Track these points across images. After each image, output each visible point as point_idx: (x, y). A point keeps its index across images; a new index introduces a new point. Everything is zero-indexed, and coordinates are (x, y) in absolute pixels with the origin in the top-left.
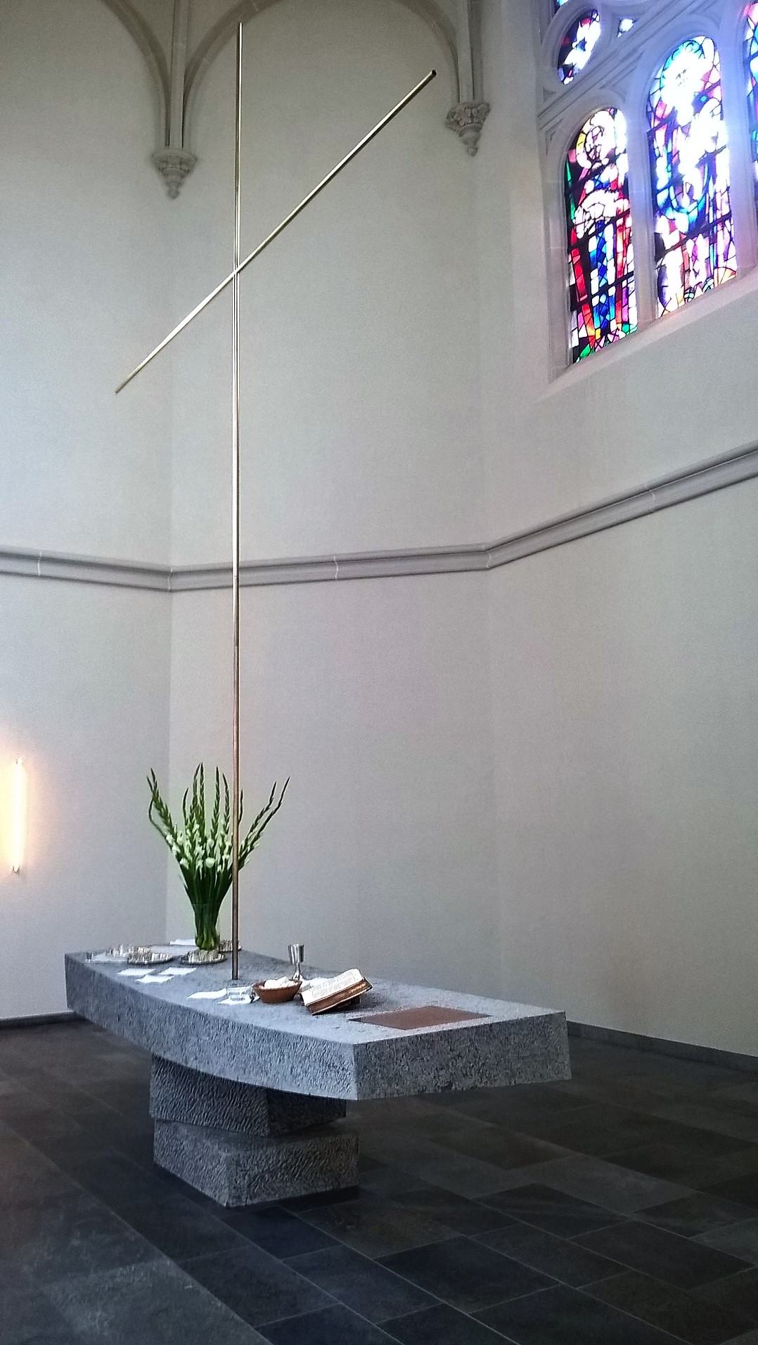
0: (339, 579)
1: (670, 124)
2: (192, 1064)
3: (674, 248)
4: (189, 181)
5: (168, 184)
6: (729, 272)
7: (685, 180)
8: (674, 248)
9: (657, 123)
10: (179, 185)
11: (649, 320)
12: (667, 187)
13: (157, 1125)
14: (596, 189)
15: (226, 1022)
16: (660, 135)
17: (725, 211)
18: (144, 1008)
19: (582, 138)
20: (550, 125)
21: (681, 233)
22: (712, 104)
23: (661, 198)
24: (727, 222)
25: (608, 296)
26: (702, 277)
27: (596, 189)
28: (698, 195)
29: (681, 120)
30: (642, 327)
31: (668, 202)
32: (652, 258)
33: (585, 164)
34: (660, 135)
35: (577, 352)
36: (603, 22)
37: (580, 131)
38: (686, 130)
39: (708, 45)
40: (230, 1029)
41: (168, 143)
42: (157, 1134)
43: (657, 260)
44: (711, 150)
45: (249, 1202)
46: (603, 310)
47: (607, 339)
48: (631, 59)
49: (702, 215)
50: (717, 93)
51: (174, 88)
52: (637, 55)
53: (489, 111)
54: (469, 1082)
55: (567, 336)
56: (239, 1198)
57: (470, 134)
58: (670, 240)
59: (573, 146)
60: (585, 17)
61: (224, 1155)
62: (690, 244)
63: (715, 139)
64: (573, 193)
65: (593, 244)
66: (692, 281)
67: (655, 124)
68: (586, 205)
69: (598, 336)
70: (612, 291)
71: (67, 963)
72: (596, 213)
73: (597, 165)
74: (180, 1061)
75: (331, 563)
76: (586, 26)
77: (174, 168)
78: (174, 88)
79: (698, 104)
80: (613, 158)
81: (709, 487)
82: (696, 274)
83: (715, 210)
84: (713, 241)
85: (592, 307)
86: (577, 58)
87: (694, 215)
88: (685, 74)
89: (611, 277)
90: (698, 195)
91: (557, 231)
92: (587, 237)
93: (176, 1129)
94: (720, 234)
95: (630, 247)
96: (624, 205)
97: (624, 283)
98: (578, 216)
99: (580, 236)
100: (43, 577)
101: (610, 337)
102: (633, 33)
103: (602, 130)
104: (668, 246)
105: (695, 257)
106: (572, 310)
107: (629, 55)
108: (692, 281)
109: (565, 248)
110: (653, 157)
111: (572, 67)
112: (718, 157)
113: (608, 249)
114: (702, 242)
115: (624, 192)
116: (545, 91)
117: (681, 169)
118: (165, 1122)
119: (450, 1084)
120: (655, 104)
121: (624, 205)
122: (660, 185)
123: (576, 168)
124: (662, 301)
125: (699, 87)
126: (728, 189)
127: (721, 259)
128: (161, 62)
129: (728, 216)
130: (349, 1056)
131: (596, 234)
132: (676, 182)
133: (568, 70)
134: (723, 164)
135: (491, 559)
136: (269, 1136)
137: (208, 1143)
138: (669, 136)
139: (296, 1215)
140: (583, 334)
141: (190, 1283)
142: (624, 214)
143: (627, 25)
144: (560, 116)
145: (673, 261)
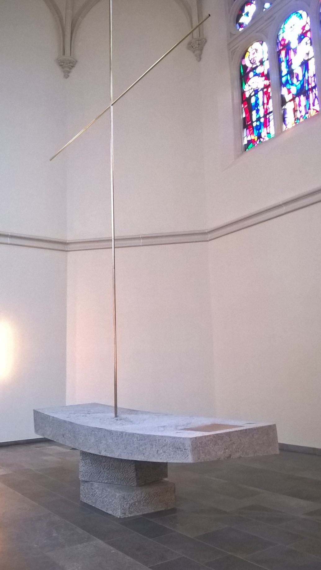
0: (142, 246)
1: (287, 47)
2: (103, 454)
3: (290, 101)
4: (74, 70)
5: (64, 72)
6: (315, 111)
7: (294, 72)
8: (290, 101)
9: (281, 48)
10: (69, 72)
11: (279, 132)
12: (287, 75)
13: (82, 484)
14: (254, 76)
15: (122, 433)
16: (283, 53)
17: (313, 85)
18: (77, 430)
19: (247, 54)
20: (234, 48)
21: (293, 95)
22: (306, 40)
23: (284, 79)
24: (314, 90)
25: (260, 122)
26: (303, 113)
27: (254, 76)
28: (301, 78)
29: (293, 46)
30: (277, 135)
31: (287, 82)
32: (280, 106)
33: (249, 65)
34: (283, 53)
35: (247, 146)
36: (256, 4)
37: (247, 51)
38: (295, 51)
39: (304, 14)
40: (124, 436)
41: (64, 54)
42: (82, 487)
43: (282, 106)
44: (306, 59)
45: (129, 516)
46: (258, 128)
47: (260, 141)
48: (270, 20)
49: (303, 86)
50: (309, 34)
51: (68, 30)
52: (272, 18)
53: (206, 42)
54: (238, 455)
55: (242, 139)
56: (125, 514)
57: (197, 52)
58: (288, 97)
59: (244, 57)
60: (249, 3)
61: (118, 494)
62: (297, 99)
63: (308, 54)
64: (244, 77)
65: (253, 100)
66: (298, 115)
67: (282, 49)
68: (250, 82)
69: (256, 139)
70: (262, 120)
71: (34, 414)
72: (255, 87)
73: (254, 66)
74: (96, 452)
75: (139, 238)
76: (249, 6)
77: (67, 65)
78: (68, 30)
79: (300, 39)
80: (262, 63)
81: (302, 205)
82: (300, 112)
83: (308, 84)
84: (308, 98)
85: (253, 127)
86: (245, 20)
87: (299, 86)
88: (294, 26)
89: (262, 113)
90: (301, 78)
91: (237, 95)
92: (250, 97)
93: (92, 485)
94: (311, 95)
95: (271, 101)
96: (267, 82)
97: (268, 116)
98: (246, 88)
99: (247, 96)
100: (10, 244)
101: (262, 140)
102: (270, 9)
103: (256, 50)
104: (287, 100)
105: (300, 105)
106: (244, 128)
107: (269, 19)
108: (298, 115)
109: (240, 101)
110: (280, 62)
111: (243, 24)
112: (309, 62)
113: (260, 102)
114: (303, 98)
115: (267, 77)
116: (231, 33)
117: (293, 67)
118: (86, 482)
119: (230, 455)
120: (280, 39)
121: (267, 82)
122: (283, 74)
123: (245, 67)
124: (285, 124)
125: (300, 31)
126: (314, 75)
127: (311, 105)
128: (61, 19)
129: (315, 87)
130: (188, 443)
131: (254, 95)
132: (291, 72)
133: (241, 25)
134: (312, 65)
135: (210, 236)
136: (136, 486)
137: (109, 490)
138: (287, 54)
139: (151, 520)
140: (249, 138)
141: (114, 550)
142: (267, 87)
143: (267, 5)
144: (237, 46)
145: (289, 107)
